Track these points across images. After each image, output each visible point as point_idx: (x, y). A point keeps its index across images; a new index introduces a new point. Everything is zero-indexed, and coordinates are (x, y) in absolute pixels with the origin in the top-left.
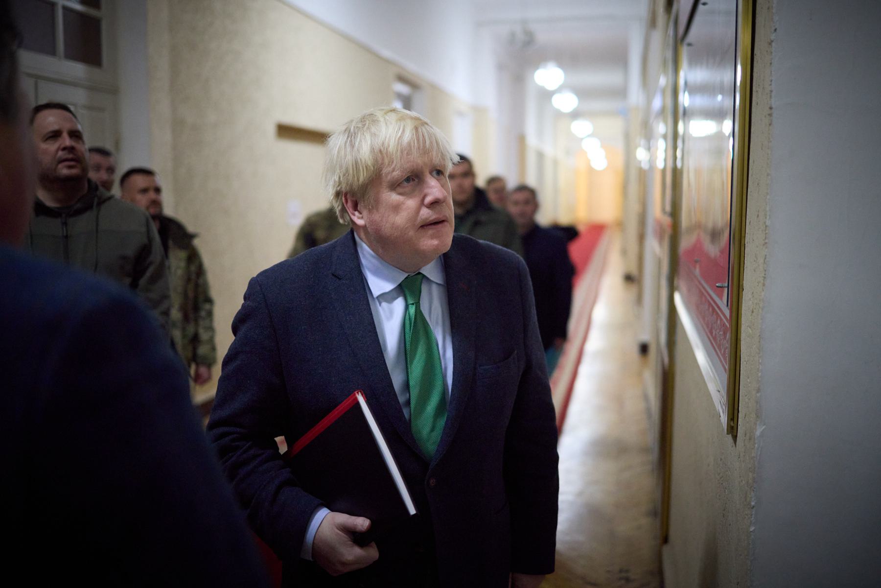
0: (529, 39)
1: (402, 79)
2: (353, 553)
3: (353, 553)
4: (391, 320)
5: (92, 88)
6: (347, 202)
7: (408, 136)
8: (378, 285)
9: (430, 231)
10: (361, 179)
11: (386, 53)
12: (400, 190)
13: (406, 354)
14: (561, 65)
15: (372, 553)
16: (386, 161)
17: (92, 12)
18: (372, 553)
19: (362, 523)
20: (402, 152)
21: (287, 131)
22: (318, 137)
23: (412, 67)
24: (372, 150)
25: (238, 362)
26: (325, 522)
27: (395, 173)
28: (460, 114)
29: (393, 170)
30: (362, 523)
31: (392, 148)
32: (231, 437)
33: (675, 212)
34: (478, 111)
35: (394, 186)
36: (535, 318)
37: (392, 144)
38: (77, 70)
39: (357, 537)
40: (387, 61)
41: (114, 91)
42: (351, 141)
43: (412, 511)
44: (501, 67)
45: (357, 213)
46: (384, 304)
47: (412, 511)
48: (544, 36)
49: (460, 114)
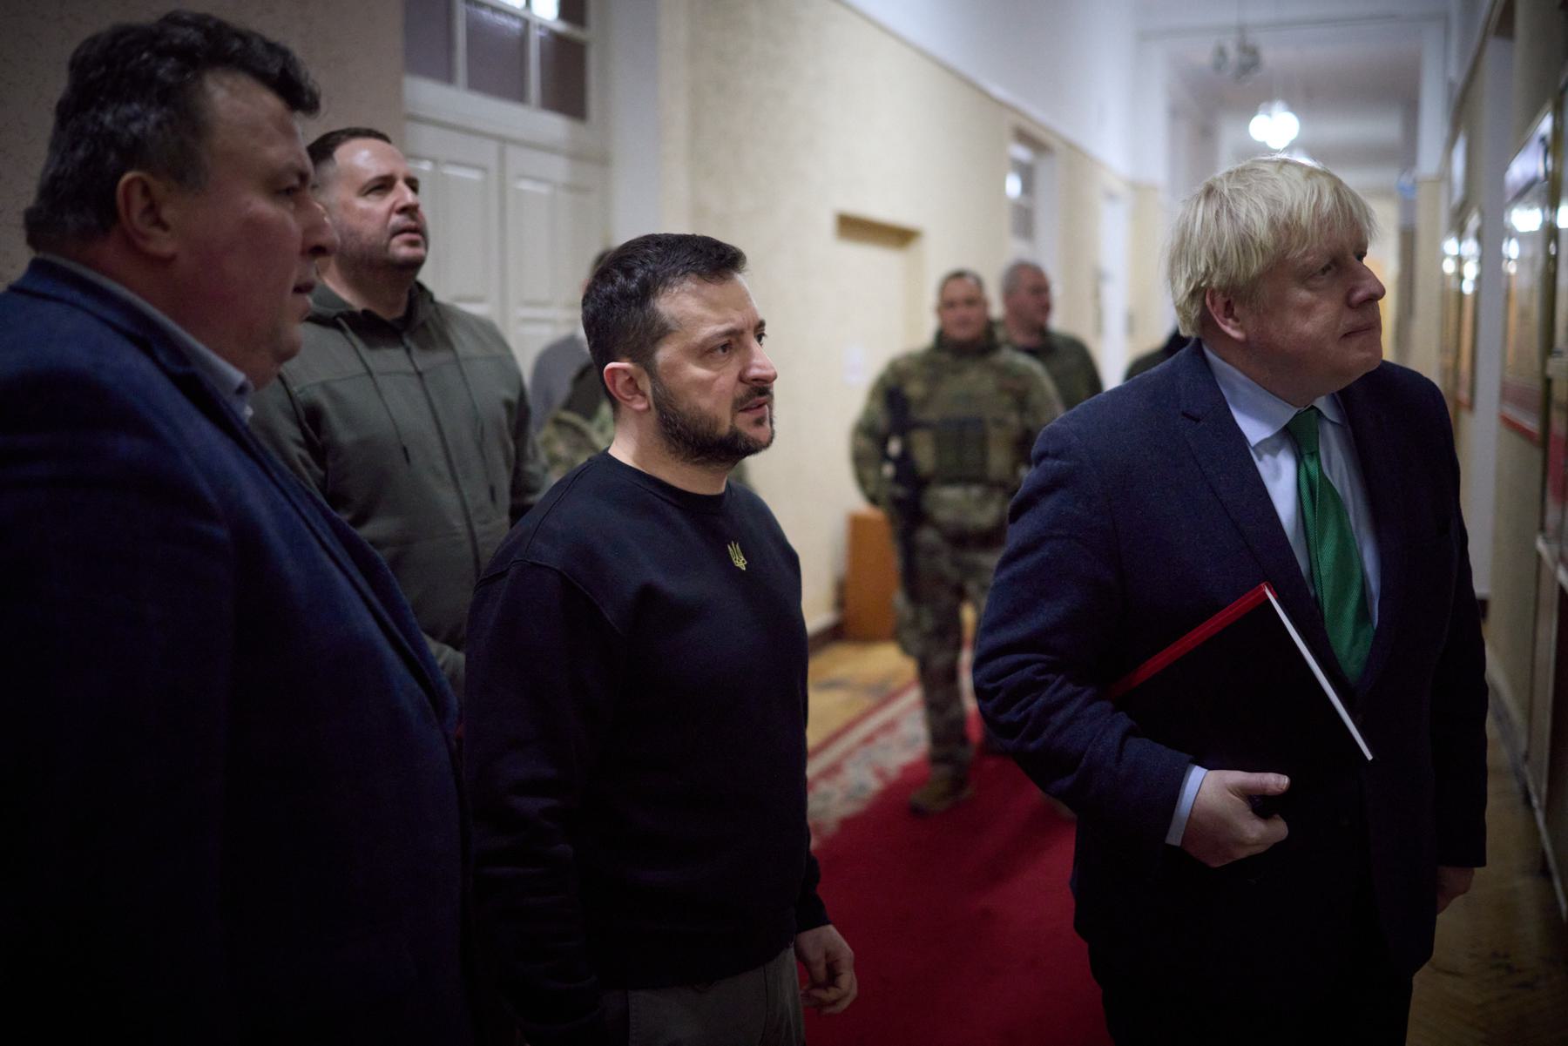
0: (1250, 60)
1: (1023, 137)
2: (1257, 832)
3: (1257, 832)
4: (1281, 481)
5: (577, 156)
6: (1213, 303)
7: (1328, 200)
8: (1254, 431)
9: (1356, 342)
10: (1254, 268)
11: (998, 91)
12: (1313, 283)
13: (1307, 539)
14: (1292, 107)
15: (1278, 829)
16: (1295, 240)
17: (577, 33)
18: (1278, 829)
19: (1276, 781)
20: (1320, 225)
21: (854, 227)
22: (900, 237)
23: (1038, 113)
24: (1272, 223)
25: (1044, 553)
26: (1205, 787)
27: (1309, 259)
28: (1111, 196)
29: (1306, 254)
30: (1276, 781)
31: (1306, 216)
32: (1034, 667)
33: (475, 549)
34: (1138, 188)
35: (1305, 277)
36: (1351, 517)
37: (1304, 215)
38: (554, 126)
39: (1261, 804)
40: (1001, 104)
41: (602, 160)
42: (1230, 211)
43: (1370, 757)
44: (1175, 112)
45: (1230, 321)
46: (1267, 457)
47: (1370, 757)
48: (1276, 54)
49: (1111, 196)
